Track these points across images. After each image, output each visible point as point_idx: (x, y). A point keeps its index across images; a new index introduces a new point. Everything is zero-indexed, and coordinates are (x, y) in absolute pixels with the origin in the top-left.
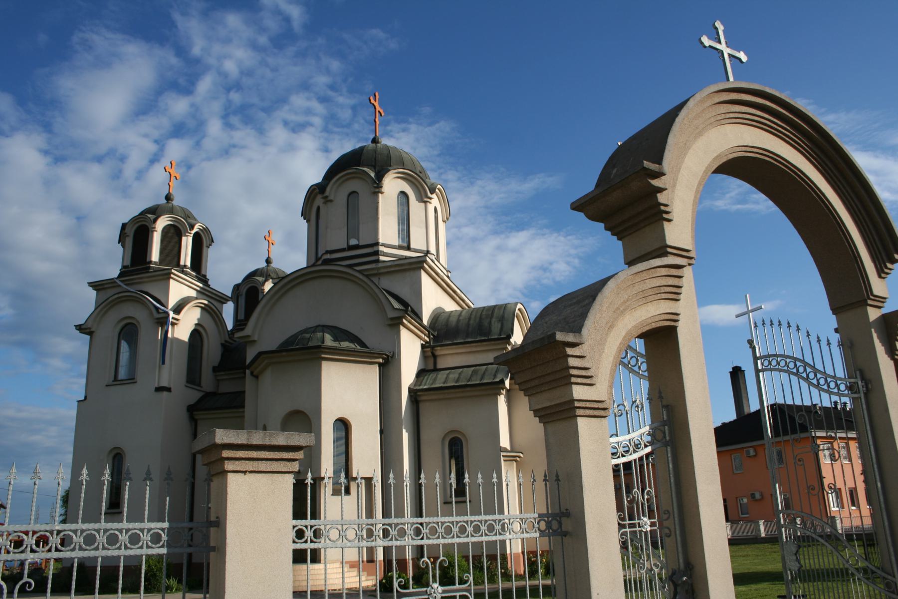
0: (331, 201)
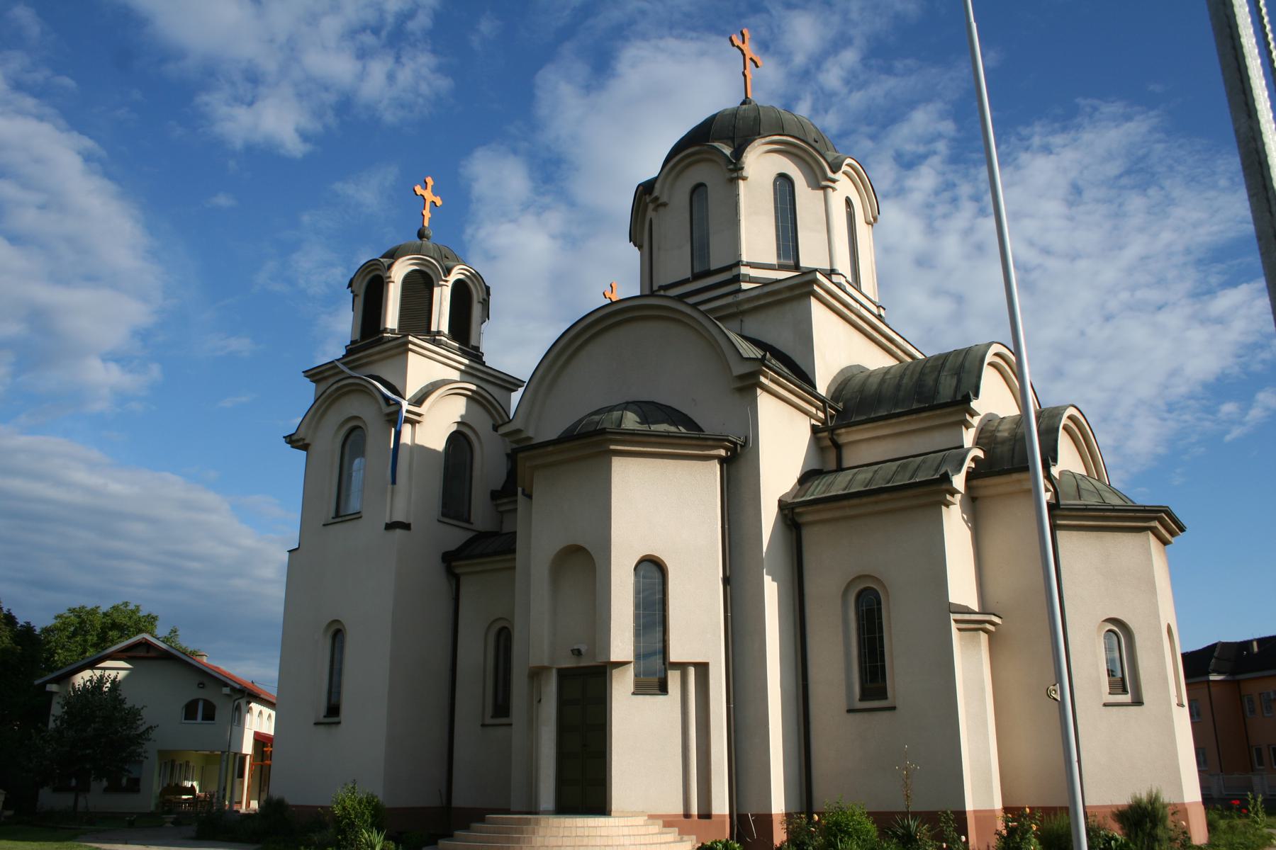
0: (664, 205)
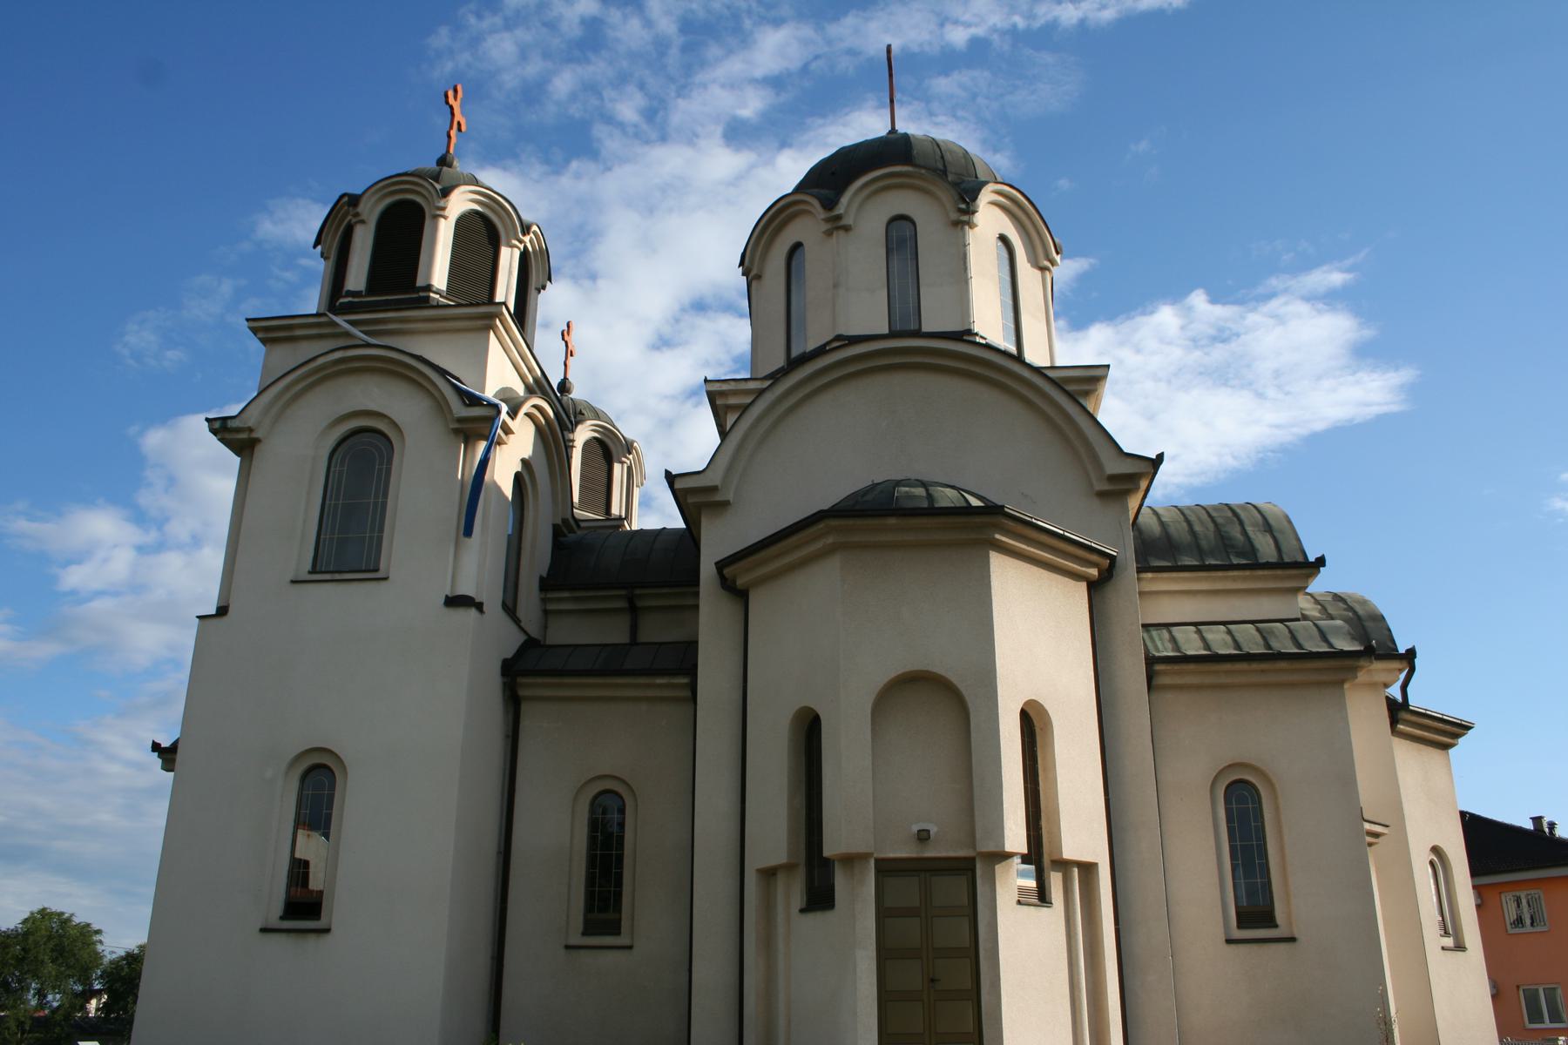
0: (847, 229)
